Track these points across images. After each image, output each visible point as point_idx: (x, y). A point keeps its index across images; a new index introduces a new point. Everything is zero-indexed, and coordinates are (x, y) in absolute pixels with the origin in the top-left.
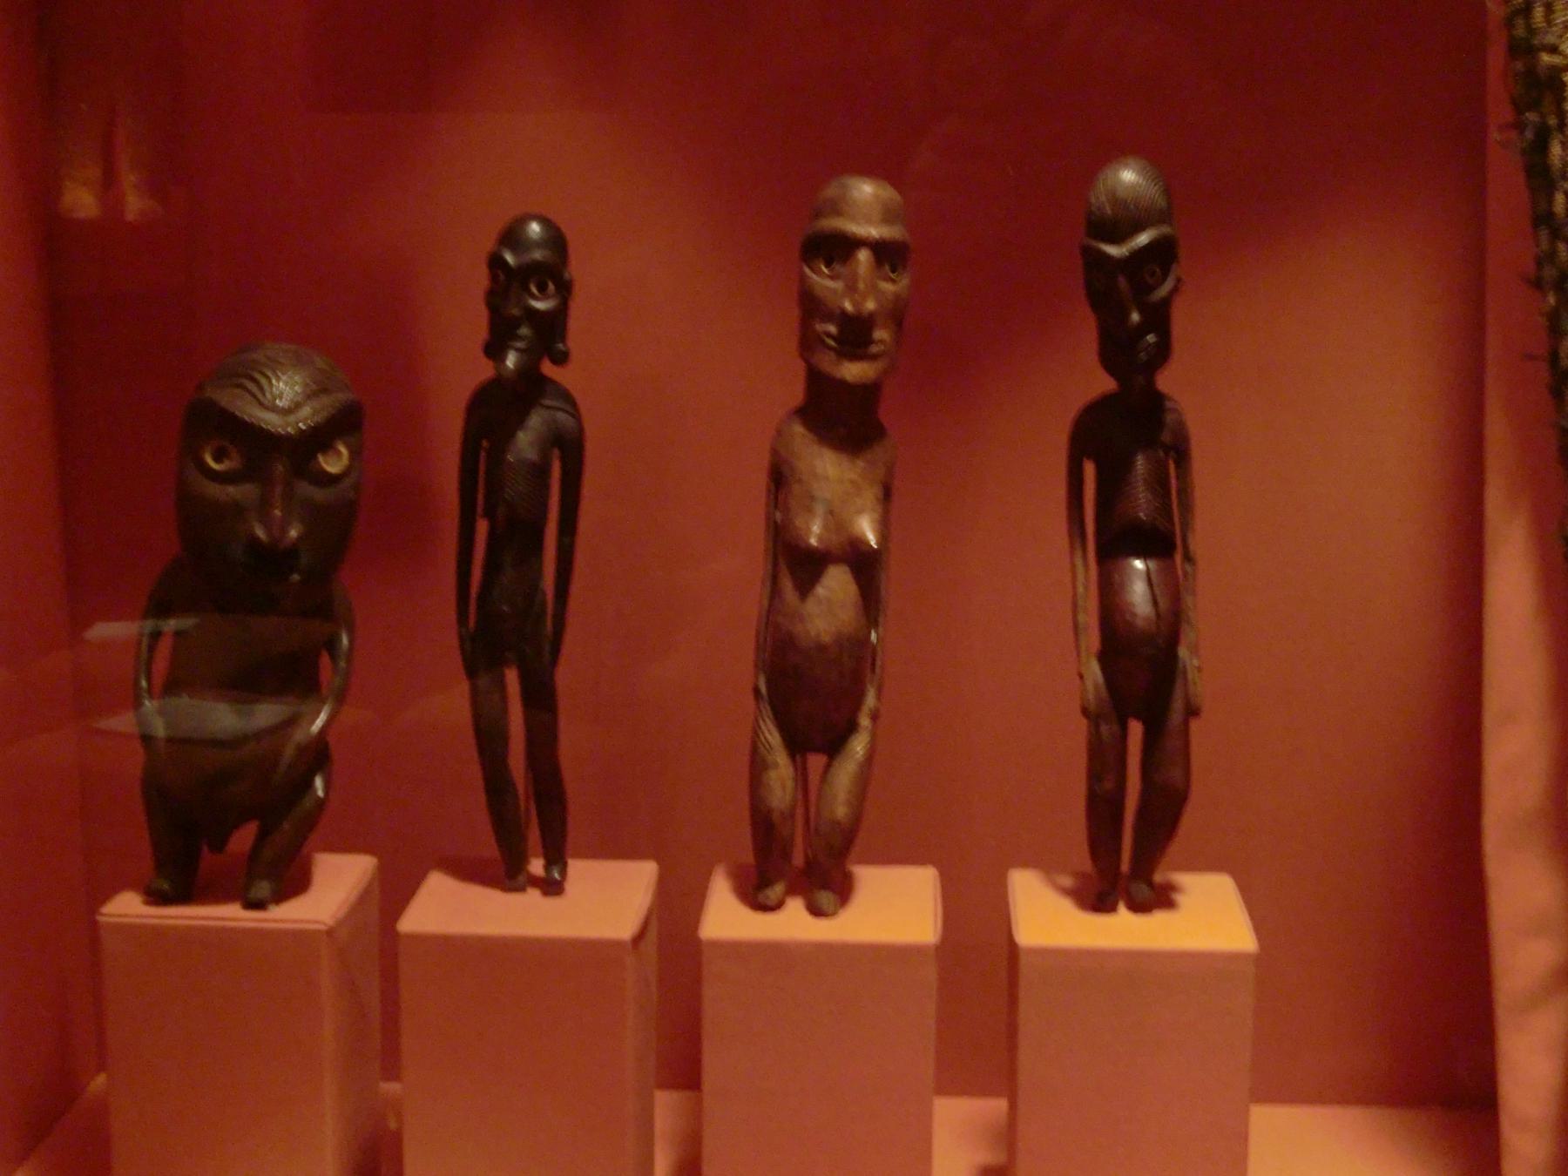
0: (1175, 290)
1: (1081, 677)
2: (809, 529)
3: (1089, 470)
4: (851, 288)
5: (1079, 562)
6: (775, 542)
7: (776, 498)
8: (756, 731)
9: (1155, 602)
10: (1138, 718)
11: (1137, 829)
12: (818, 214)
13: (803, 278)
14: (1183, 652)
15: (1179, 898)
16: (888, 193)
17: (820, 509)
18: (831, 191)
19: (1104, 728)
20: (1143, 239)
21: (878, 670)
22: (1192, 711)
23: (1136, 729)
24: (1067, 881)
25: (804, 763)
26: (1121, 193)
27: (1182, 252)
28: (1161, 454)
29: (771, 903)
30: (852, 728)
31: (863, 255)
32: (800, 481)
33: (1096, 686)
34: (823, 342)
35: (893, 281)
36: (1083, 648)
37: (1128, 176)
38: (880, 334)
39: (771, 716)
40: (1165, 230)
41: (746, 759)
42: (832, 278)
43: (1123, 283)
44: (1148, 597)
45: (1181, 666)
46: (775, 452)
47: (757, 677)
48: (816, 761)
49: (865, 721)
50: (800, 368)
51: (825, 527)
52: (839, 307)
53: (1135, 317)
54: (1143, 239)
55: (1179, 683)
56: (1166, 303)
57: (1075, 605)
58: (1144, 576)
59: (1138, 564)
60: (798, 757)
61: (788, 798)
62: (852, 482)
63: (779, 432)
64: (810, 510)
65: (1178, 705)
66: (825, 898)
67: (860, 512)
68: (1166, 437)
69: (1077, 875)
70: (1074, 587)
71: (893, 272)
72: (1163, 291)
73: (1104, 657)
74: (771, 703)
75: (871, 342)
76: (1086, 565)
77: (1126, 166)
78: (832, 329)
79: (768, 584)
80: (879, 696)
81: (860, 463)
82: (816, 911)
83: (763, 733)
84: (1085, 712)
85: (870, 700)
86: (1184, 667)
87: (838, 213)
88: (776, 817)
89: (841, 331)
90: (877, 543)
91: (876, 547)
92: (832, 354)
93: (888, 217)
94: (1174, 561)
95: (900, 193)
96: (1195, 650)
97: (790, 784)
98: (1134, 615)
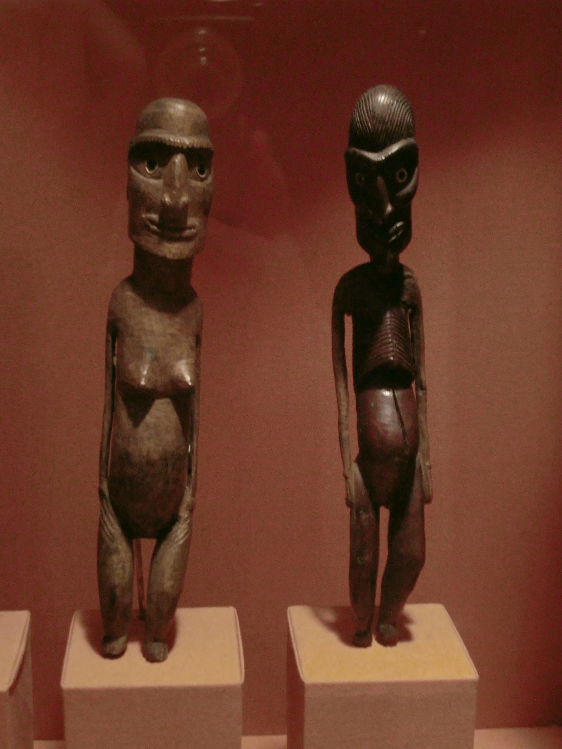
0: (415, 188)
1: (346, 478)
2: (140, 373)
3: (348, 321)
4: (169, 185)
5: (342, 391)
6: (113, 381)
7: (114, 348)
8: (101, 525)
9: (402, 423)
10: (387, 506)
11: (383, 586)
12: (141, 127)
13: (130, 177)
14: (419, 456)
15: (413, 628)
16: (197, 111)
17: (148, 356)
18: (151, 109)
19: (364, 517)
20: (395, 148)
21: (193, 474)
22: (426, 500)
23: (384, 513)
24: (330, 617)
25: (139, 547)
26: (378, 111)
27: (421, 159)
28: (403, 310)
29: (115, 653)
30: (174, 519)
31: (178, 159)
32: (132, 335)
33: (356, 483)
34: (148, 228)
35: (202, 180)
36: (347, 458)
37: (382, 99)
38: (192, 221)
39: (113, 512)
40: (411, 140)
41: (94, 545)
42: (155, 178)
43: (380, 180)
44: (396, 420)
45: (417, 467)
46: (111, 312)
47: (101, 482)
48: (148, 544)
49: (184, 514)
50: (131, 245)
51: (152, 370)
52: (161, 201)
53: (389, 208)
54: (395, 148)
55: (416, 483)
56: (410, 196)
57: (340, 424)
58: (392, 401)
59: (387, 393)
60: (134, 541)
61: (127, 575)
62: (173, 335)
63: (114, 295)
64: (140, 357)
65: (416, 495)
66: (156, 648)
67: (179, 358)
68: (405, 298)
69: (337, 609)
70: (339, 411)
71: (123, 311)
72: (408, 188)
73: (361, 460)
74: (113, 503)
75: (184, 228)
76: (347, 394)
77: (383, 92)
78: (155, 217)
79: (108, 412)
80: (193, 495)
81: (177, 320)
82: (151, 658)
83: (106, 526)
84: (349, 503)
85: (188, 498)
86: (420, 468)
87: (157, 126)
88: (118, 591)
89: (161, 218)
90: (191, 381)
91: (190, 384)
92: (156, 237)
93: (197, 129)
94: (411, 388)
95: (206, 114)
96: (426, 456)
97: (128, 565)
98: (386, 432)
